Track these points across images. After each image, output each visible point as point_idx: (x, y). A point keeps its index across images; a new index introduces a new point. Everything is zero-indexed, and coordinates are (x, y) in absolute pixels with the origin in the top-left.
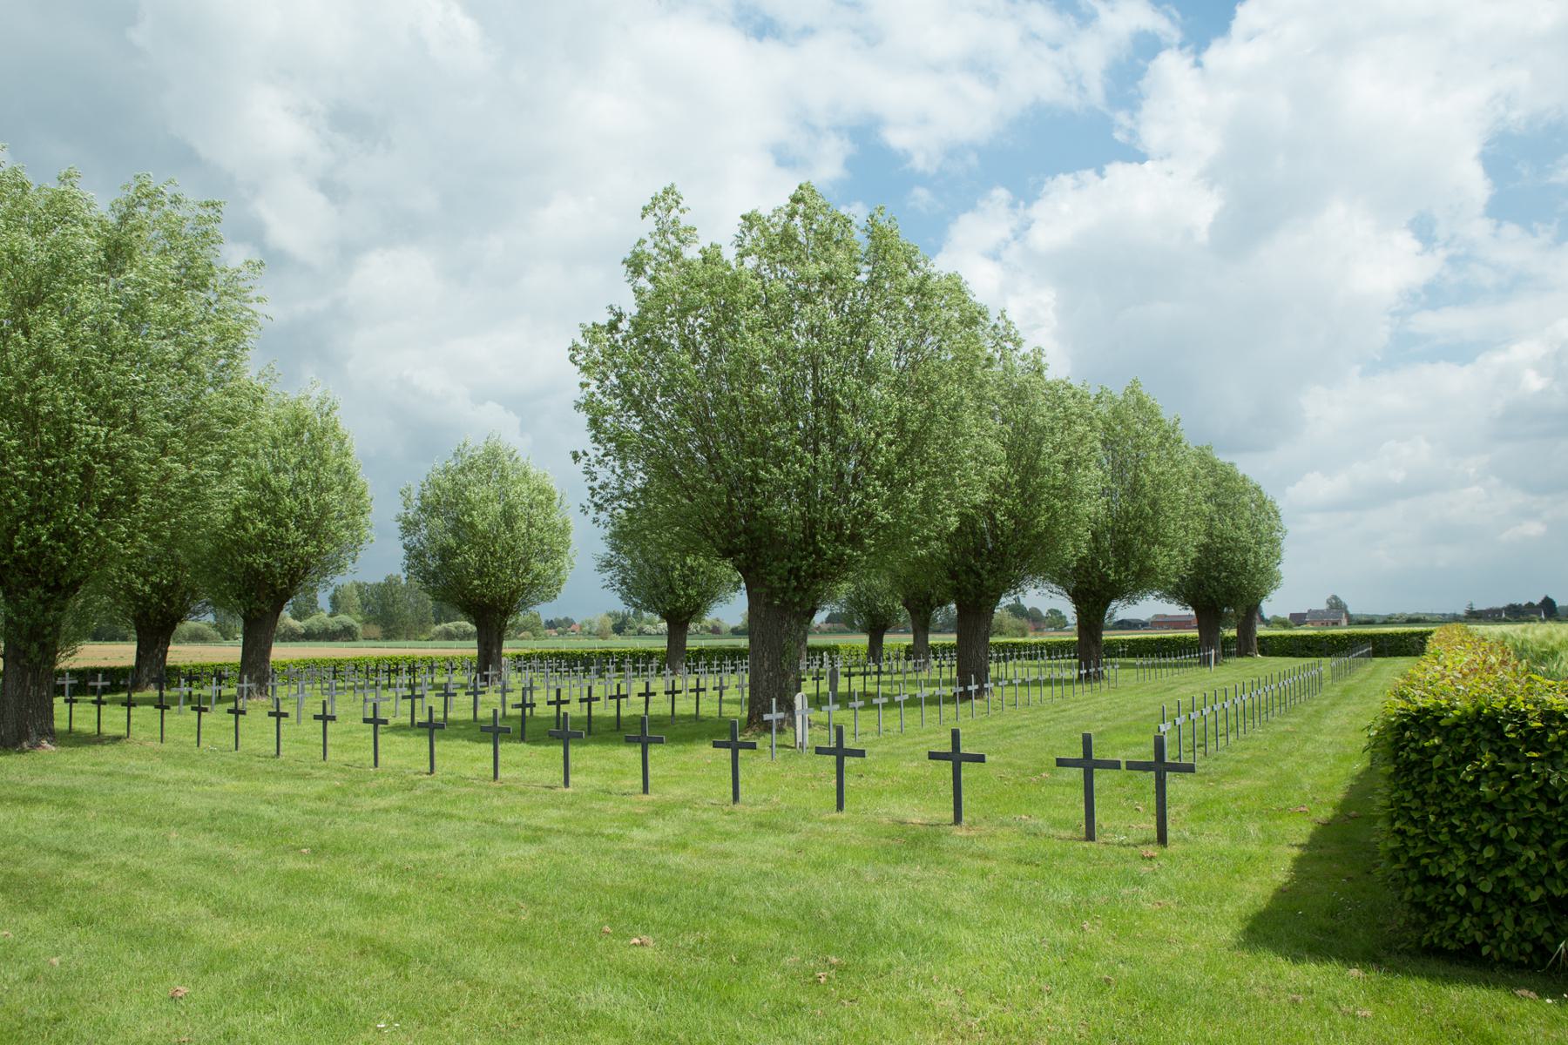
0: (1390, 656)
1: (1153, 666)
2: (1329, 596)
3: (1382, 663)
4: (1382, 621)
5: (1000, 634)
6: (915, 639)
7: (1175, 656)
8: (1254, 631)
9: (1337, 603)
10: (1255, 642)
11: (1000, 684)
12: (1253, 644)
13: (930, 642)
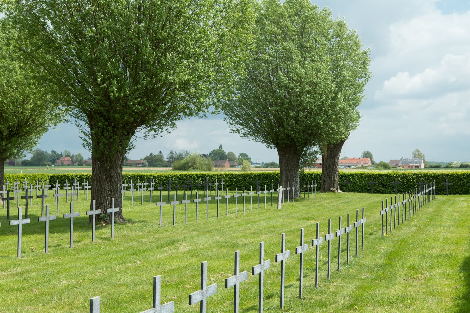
0: (451, 194)
1: (233, 200)
2: (414, 150)
3: (444, 202)
4: (445, 166)
5: (194, 169)
6: (93, 171)
7: (268, 189)
8: (336, 169)
9: (418, 155)
10: (337, 179)
11: (195, 200)
12: (335, 181)
13: (124, 173)
